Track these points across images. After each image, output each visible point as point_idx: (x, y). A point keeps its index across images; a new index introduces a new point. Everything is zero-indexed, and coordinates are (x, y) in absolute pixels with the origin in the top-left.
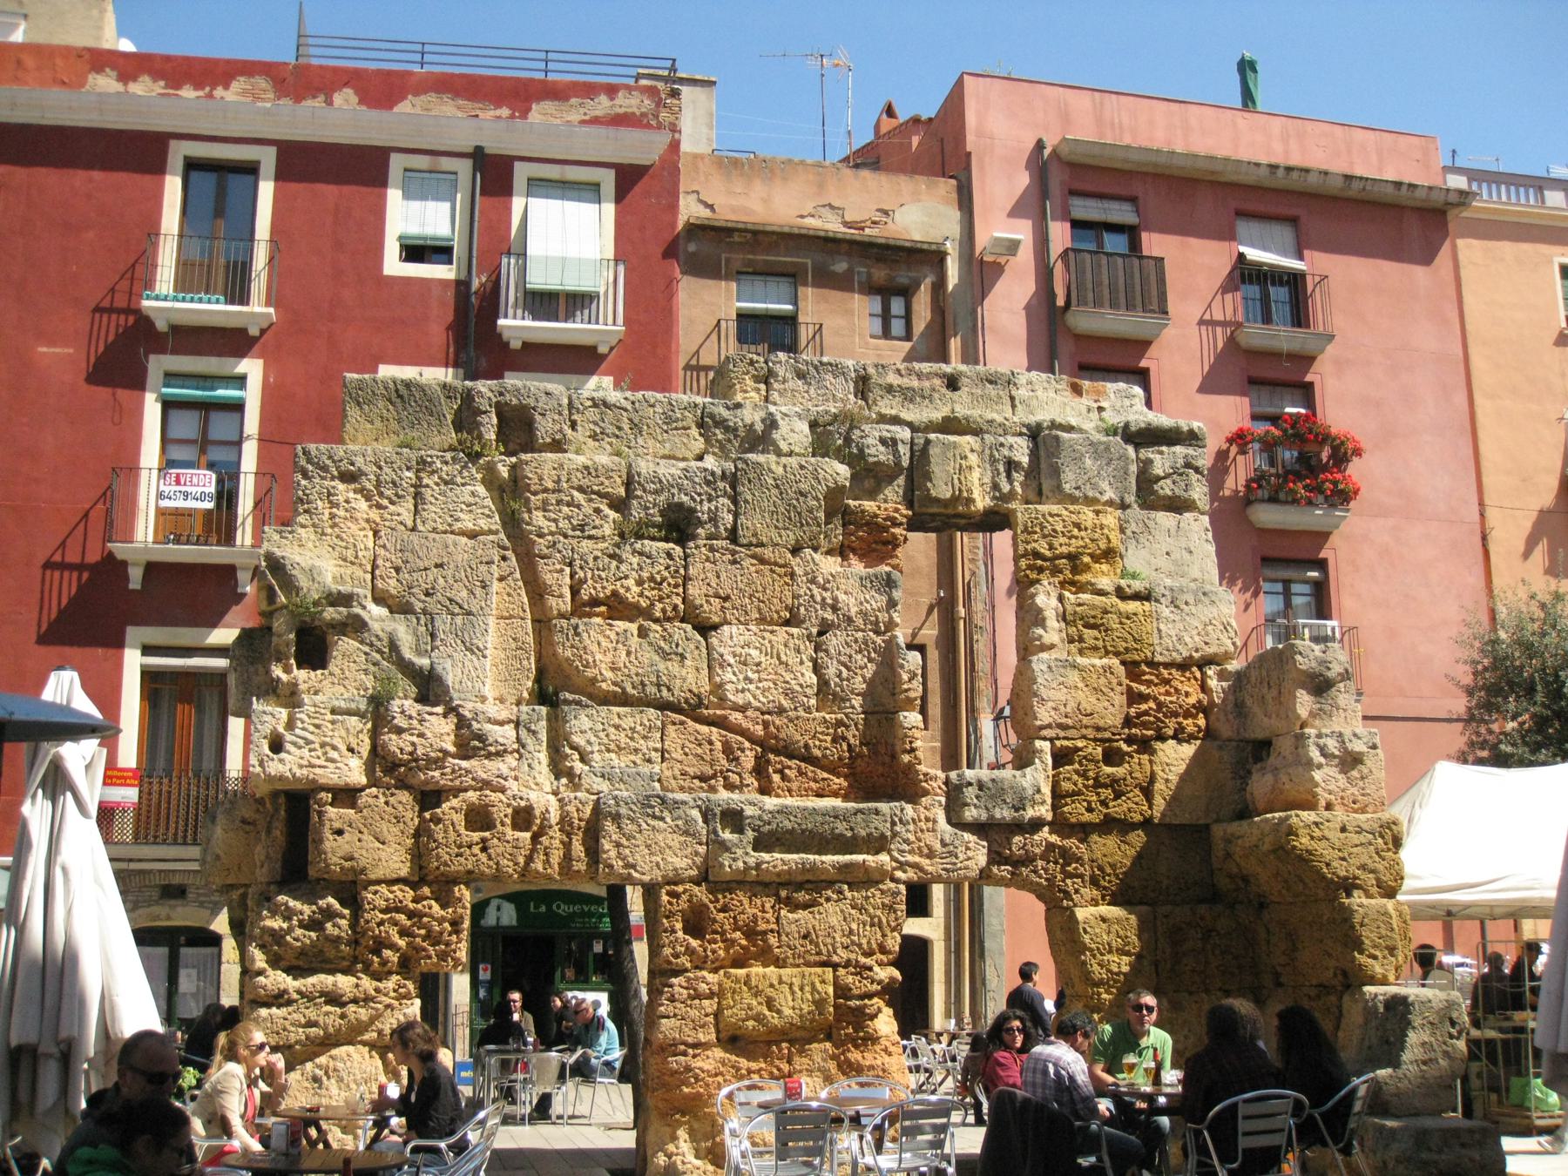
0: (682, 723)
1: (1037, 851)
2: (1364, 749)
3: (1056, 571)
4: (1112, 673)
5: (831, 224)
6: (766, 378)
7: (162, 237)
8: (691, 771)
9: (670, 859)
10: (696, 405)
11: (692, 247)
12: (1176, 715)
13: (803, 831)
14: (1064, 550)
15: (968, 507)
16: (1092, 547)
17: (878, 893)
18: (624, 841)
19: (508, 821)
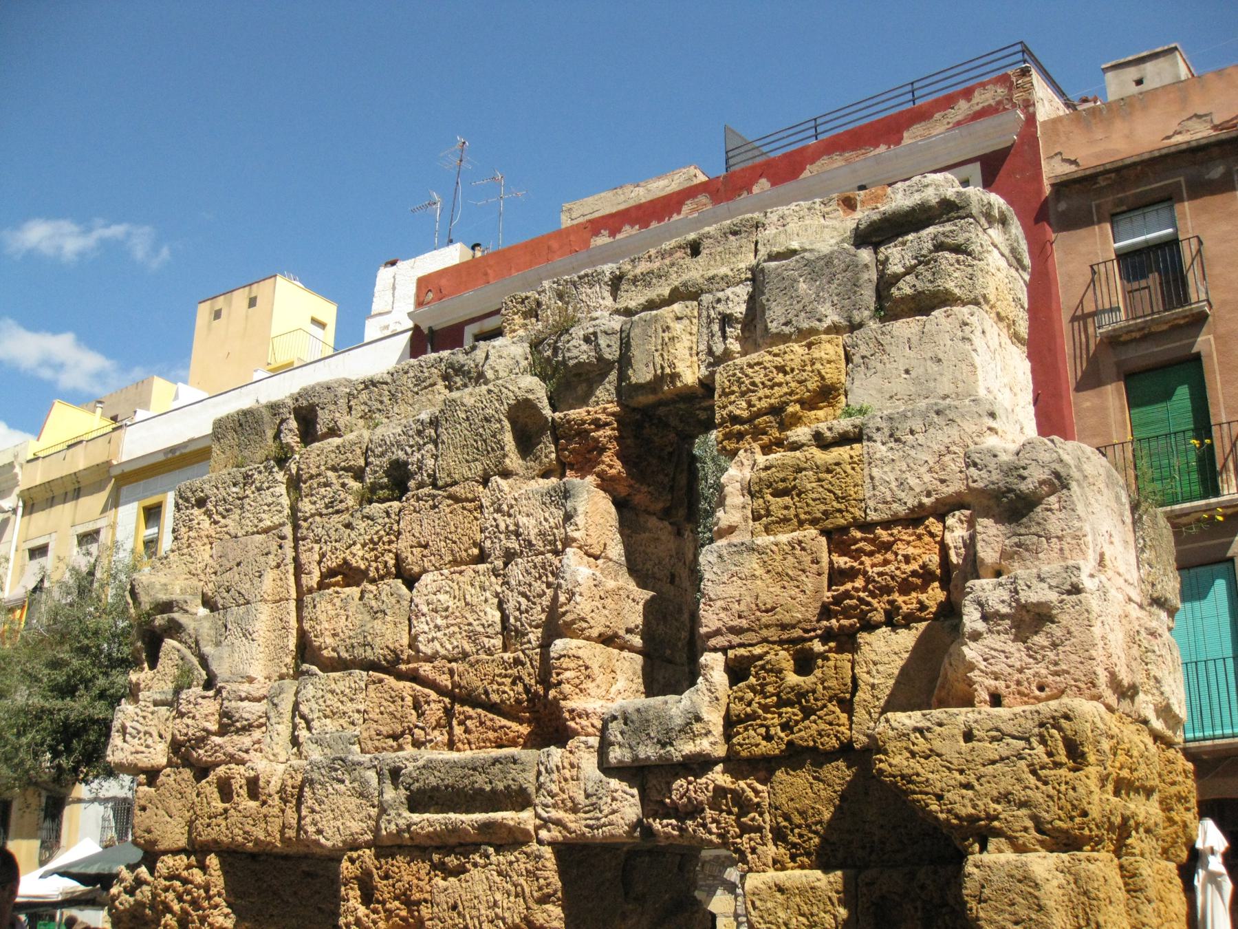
0: (381, 681)
1: (702, 797)
2: (1053, 596)
3: (757, 433)
4: (803, 549)
5: (1200, 132)
8: (385, 730)
9: (348, 824)
10: (441, 360)
11: (1062, 206)
12: (887, 590)
13: (447, 787)
14: (764, 404)
15: (674, 385)
16: (802, 393)
17: (522, 858)
18: (317, 808)
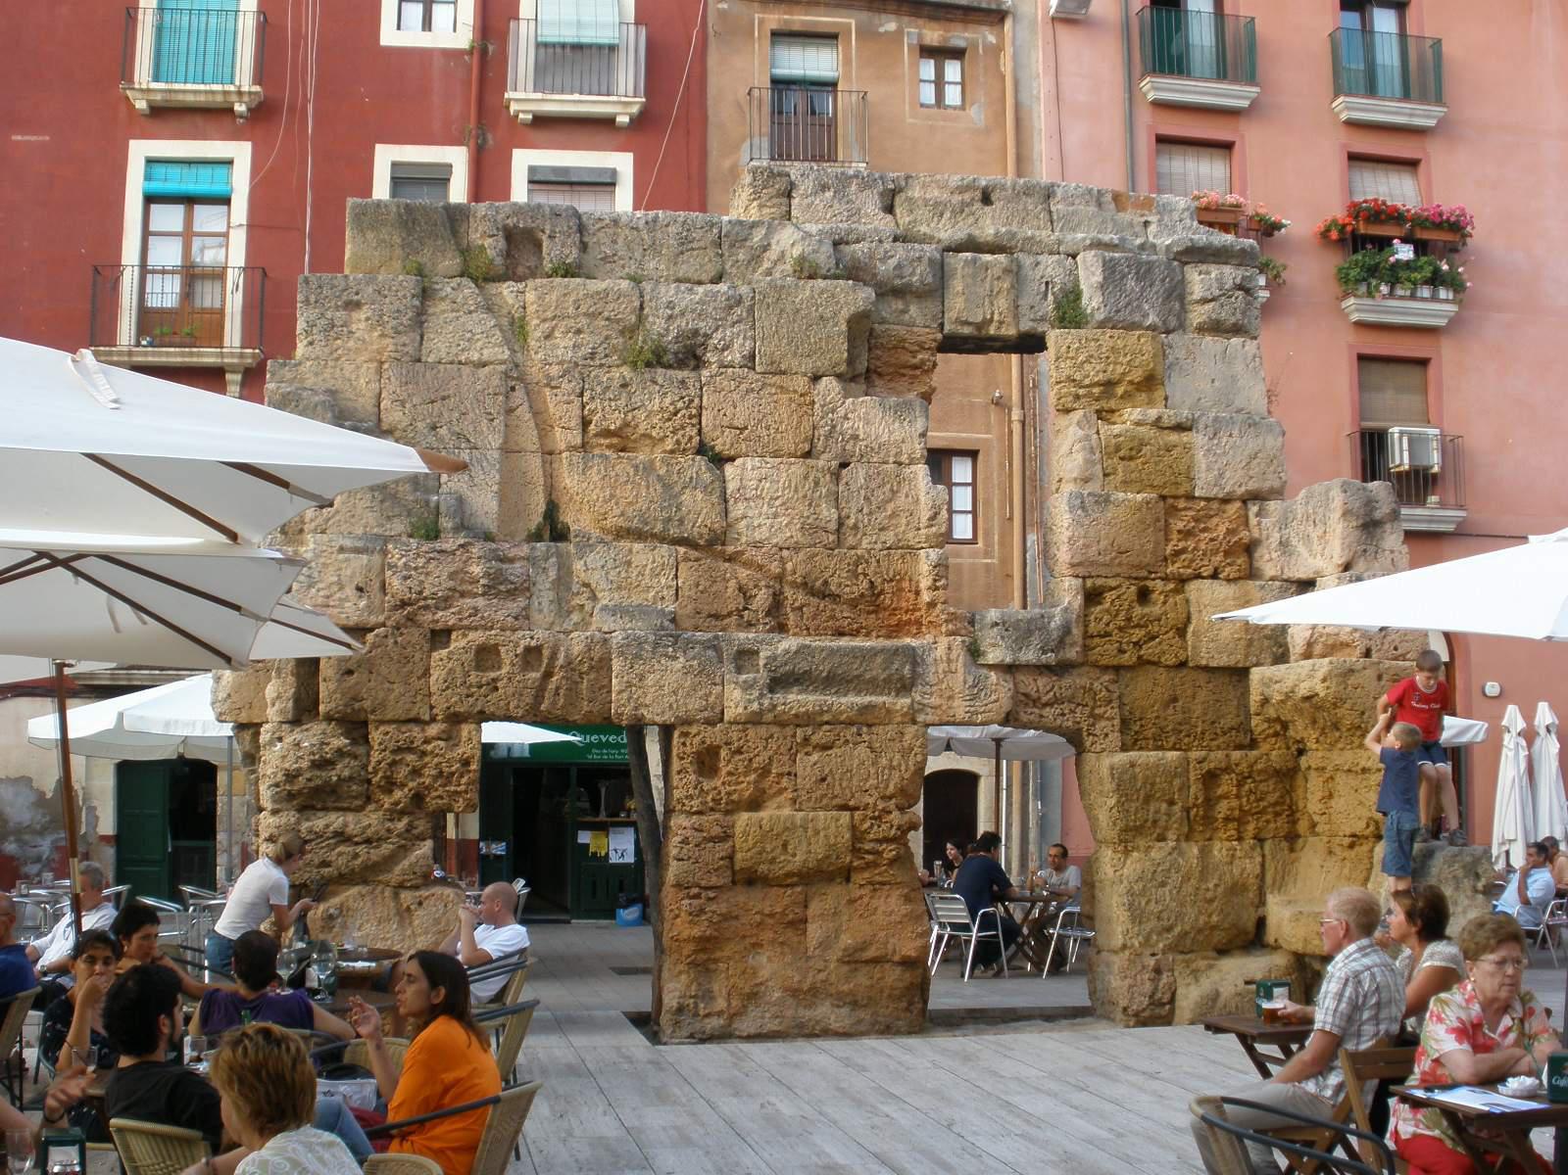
7: (141, 11)
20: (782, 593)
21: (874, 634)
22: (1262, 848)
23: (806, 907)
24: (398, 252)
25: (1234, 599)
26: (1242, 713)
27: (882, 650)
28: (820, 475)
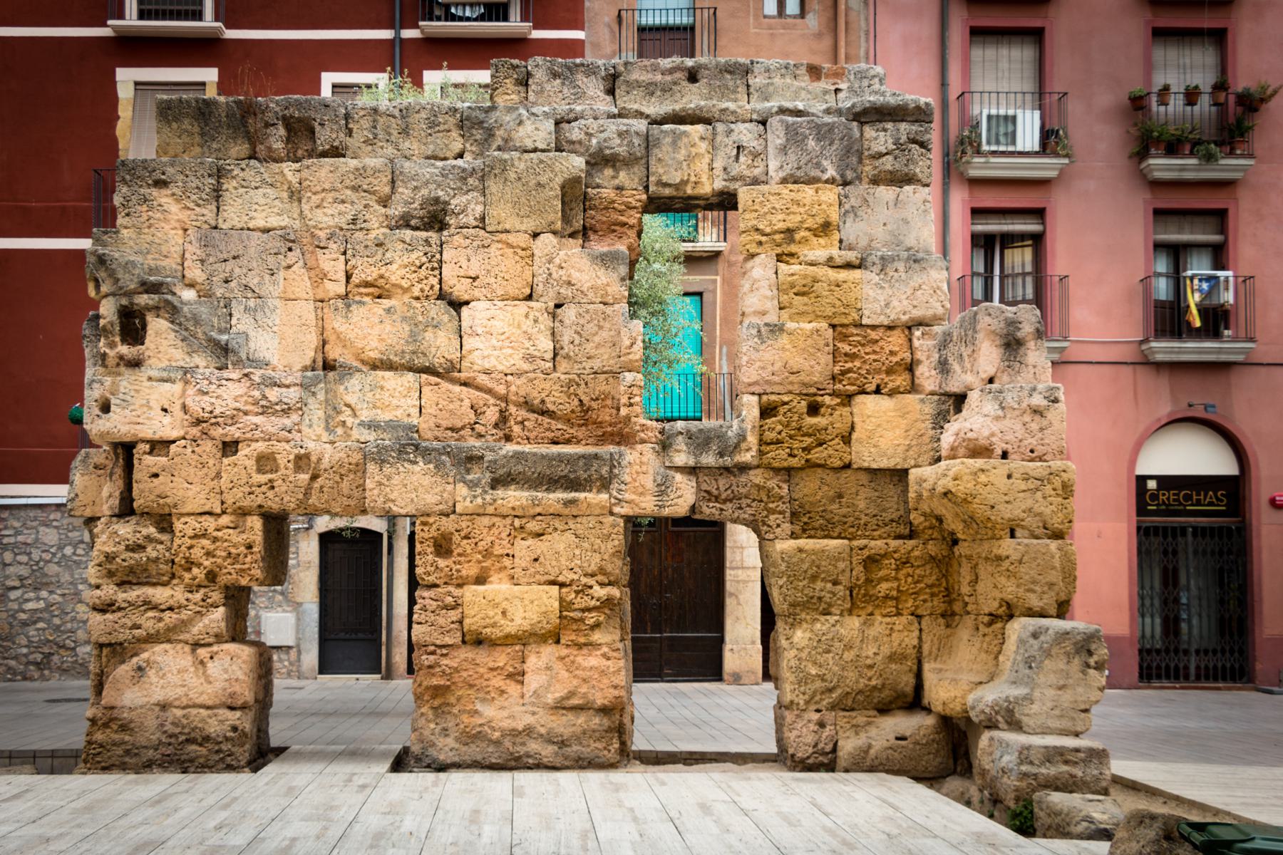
6: (524, 82)
10: (456, 110)
16: (810, 223)
18: (385, 481)
19: (291, 465)
20: (507, 410)
21: (583, 442)
22: (920, 623)
23: (523, 662)
24: (197, 139)
25: (895, 410)
26: (902, 508)
27: (583, 456)
28: (537, 314)
